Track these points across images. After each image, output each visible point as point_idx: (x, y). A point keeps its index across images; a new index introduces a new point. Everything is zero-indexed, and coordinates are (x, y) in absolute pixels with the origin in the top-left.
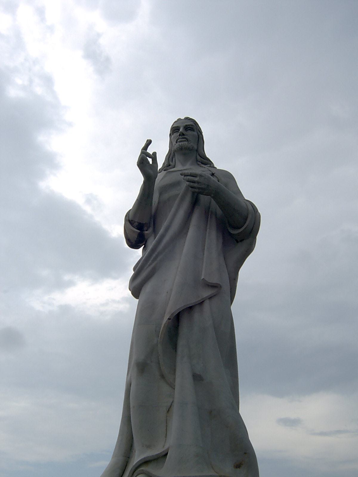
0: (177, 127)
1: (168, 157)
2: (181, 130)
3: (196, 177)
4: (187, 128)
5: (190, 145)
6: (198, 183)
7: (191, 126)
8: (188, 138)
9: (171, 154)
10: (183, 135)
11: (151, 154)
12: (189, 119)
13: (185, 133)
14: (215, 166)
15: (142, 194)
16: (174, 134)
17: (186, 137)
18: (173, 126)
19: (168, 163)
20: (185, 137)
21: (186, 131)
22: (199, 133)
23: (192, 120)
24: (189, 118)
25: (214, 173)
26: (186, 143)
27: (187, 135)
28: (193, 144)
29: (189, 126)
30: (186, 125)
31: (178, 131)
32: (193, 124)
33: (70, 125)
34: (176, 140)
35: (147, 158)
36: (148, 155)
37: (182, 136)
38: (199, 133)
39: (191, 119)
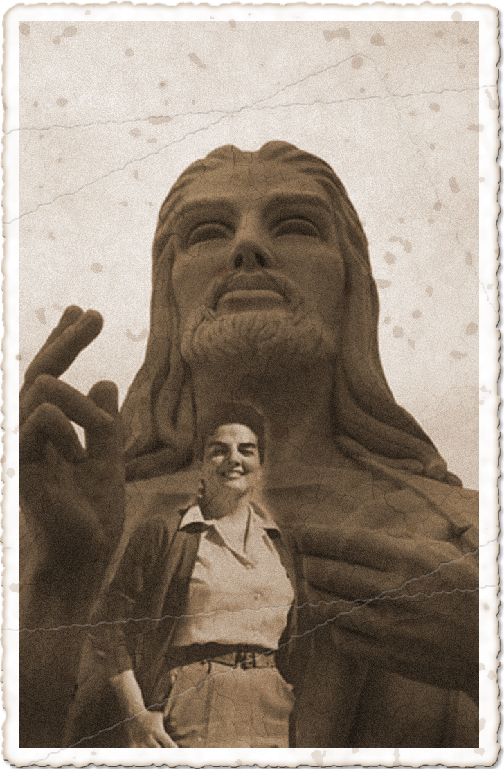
0: (222, 204)
1: (146, 389)
2: (248, 230)
3: (385, 570)
4: (287, 218)
5: (300, 326)
6: (400, 607)
7: (304, 208)
8: (292, 283)
9: (165, 372)
10: (261, 260)
11: (85, 391)
12: (290, 154)
13: (268, 246)
14: (450, 469)
15: (122, 692)
16: (194, 249)
17: (272, 273)
18: (191, 197)
19: (149, 431)
20: (273, 279)
21: (279, 234)
22: (352, 249)
23: (308, 165)
24: (291, 148)
25: (460, 525)
26: (280, 314)
27: (281, 264)
28: (309, 327)
29: (293, 208)
30: (279, 201)
31: (223, 228)
32: (324, 196)
33: (9, 548)
34: (209, 291)
35: (71, 425)
36: (66, 398)
37: (250, 269)
38: (352, 249)
39: (306, 157)
